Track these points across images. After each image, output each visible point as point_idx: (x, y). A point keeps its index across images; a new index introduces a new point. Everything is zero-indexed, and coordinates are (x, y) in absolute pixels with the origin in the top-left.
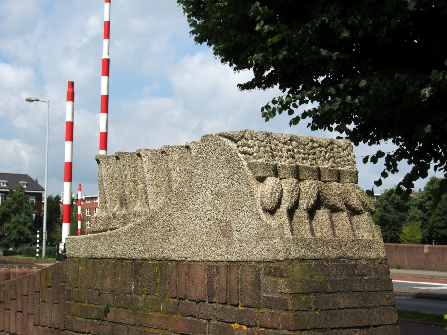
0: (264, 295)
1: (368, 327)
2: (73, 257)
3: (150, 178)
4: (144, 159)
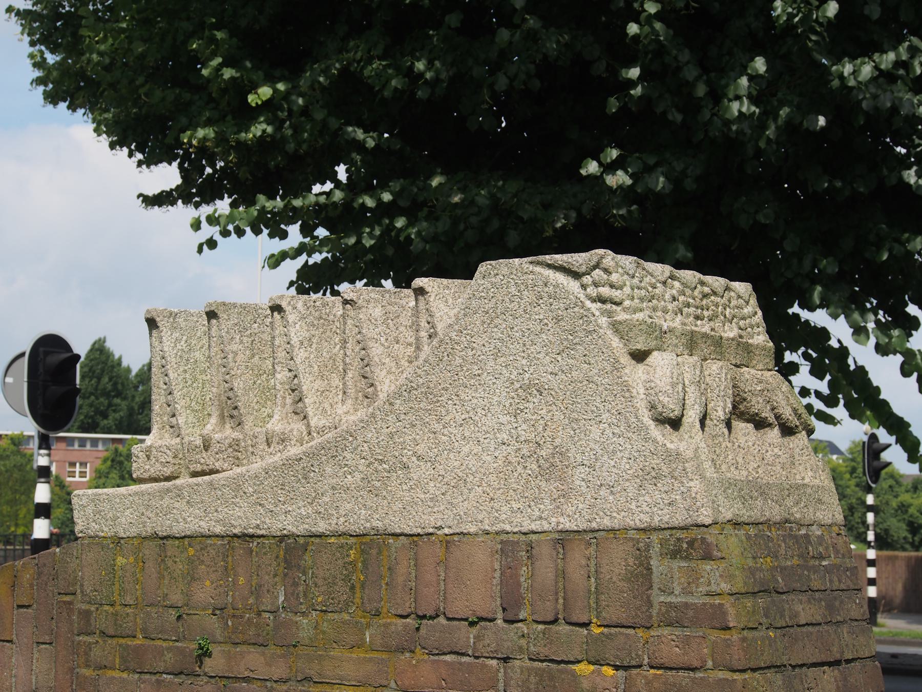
0: (662, 599)
1: (837, 663)
2: (97, 536)
3: (306, 358)
4: (291, 318)
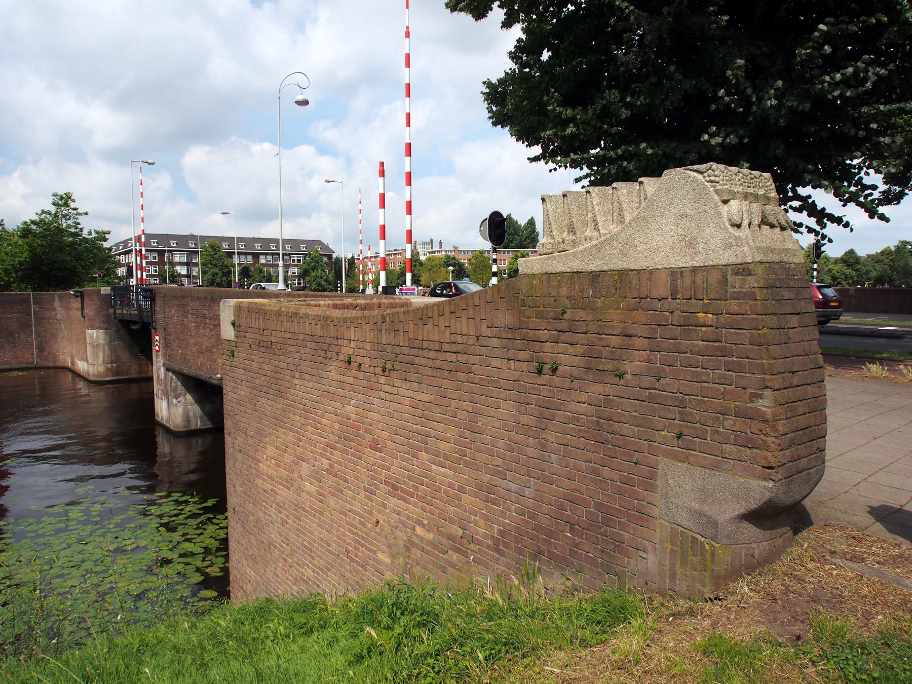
1: (799, 314)
4: (593, 195)
